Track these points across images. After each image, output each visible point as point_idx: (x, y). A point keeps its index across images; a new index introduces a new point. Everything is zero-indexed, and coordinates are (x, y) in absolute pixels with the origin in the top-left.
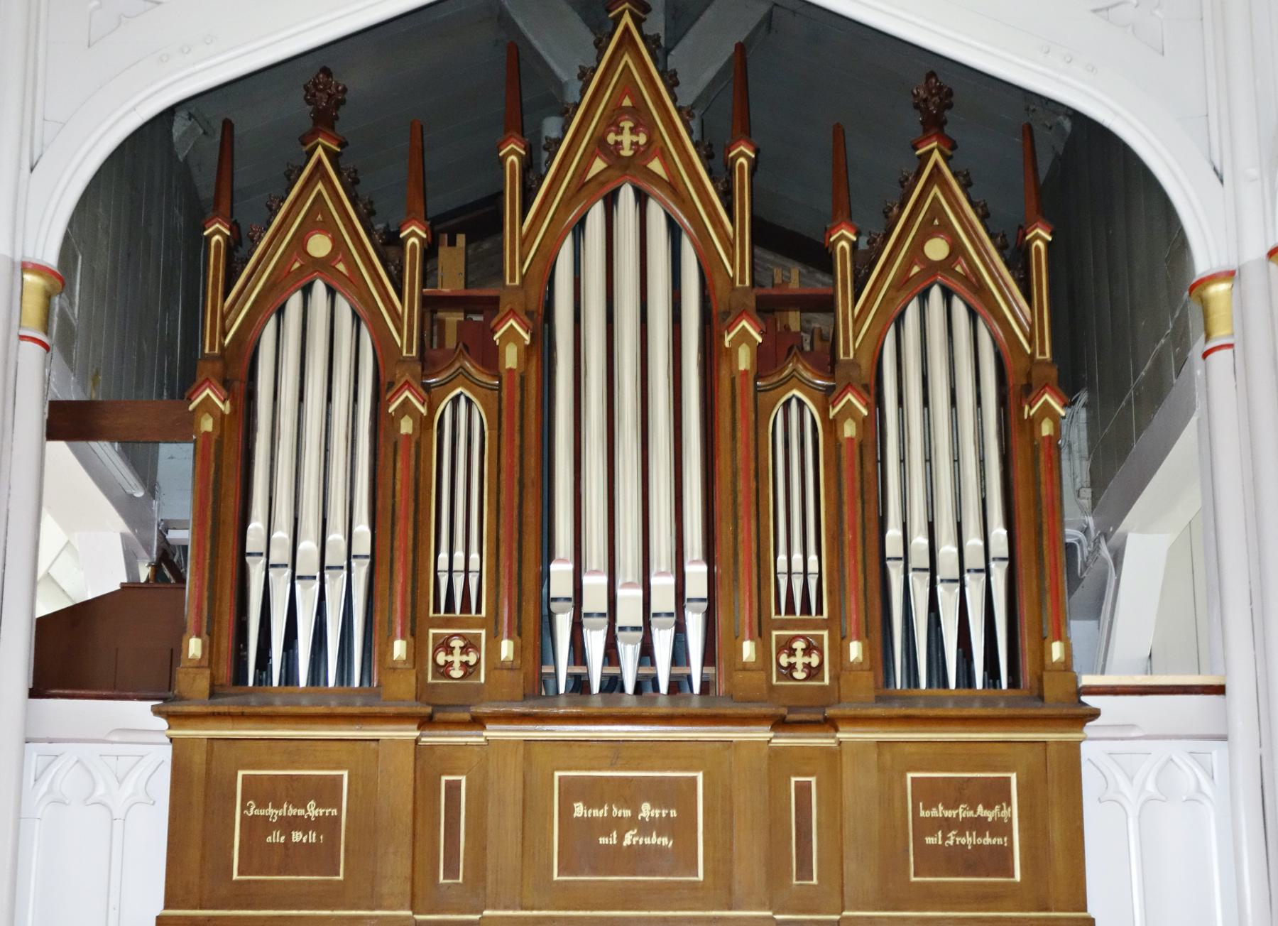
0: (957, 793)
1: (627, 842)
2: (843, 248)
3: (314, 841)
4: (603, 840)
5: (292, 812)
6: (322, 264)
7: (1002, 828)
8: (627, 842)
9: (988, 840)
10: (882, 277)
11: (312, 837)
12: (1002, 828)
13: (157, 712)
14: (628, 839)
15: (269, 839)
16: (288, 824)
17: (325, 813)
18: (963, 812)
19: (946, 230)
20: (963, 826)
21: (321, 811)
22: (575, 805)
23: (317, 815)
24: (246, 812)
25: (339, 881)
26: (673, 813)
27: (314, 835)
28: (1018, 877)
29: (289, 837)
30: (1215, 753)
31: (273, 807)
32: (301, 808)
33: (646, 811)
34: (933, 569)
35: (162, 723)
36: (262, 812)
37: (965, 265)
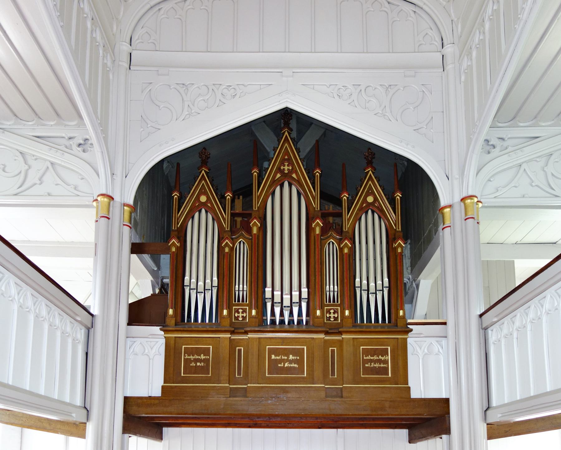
0: (374, 352)
1: (286, 366)
2: (398, 198)
4: (279, 365)
5: (197, 357)
6: (204, 205)
7: (386, 362)
8: (286, 366)
9: (382, 365)
10: (356, 207)
11: (202, 364)
12: (386, 362)
13: (161, 329)
15: (191, 365)
16: (196, 361)
18: (375, 358)
19: (373, 194)
20: (375, 361)
21: (205, 357)
24: (185, 357)
29: (196, 364)
33: (291, 357)
34: (368, 290)
35: (162, 333)
36: (189, 357)
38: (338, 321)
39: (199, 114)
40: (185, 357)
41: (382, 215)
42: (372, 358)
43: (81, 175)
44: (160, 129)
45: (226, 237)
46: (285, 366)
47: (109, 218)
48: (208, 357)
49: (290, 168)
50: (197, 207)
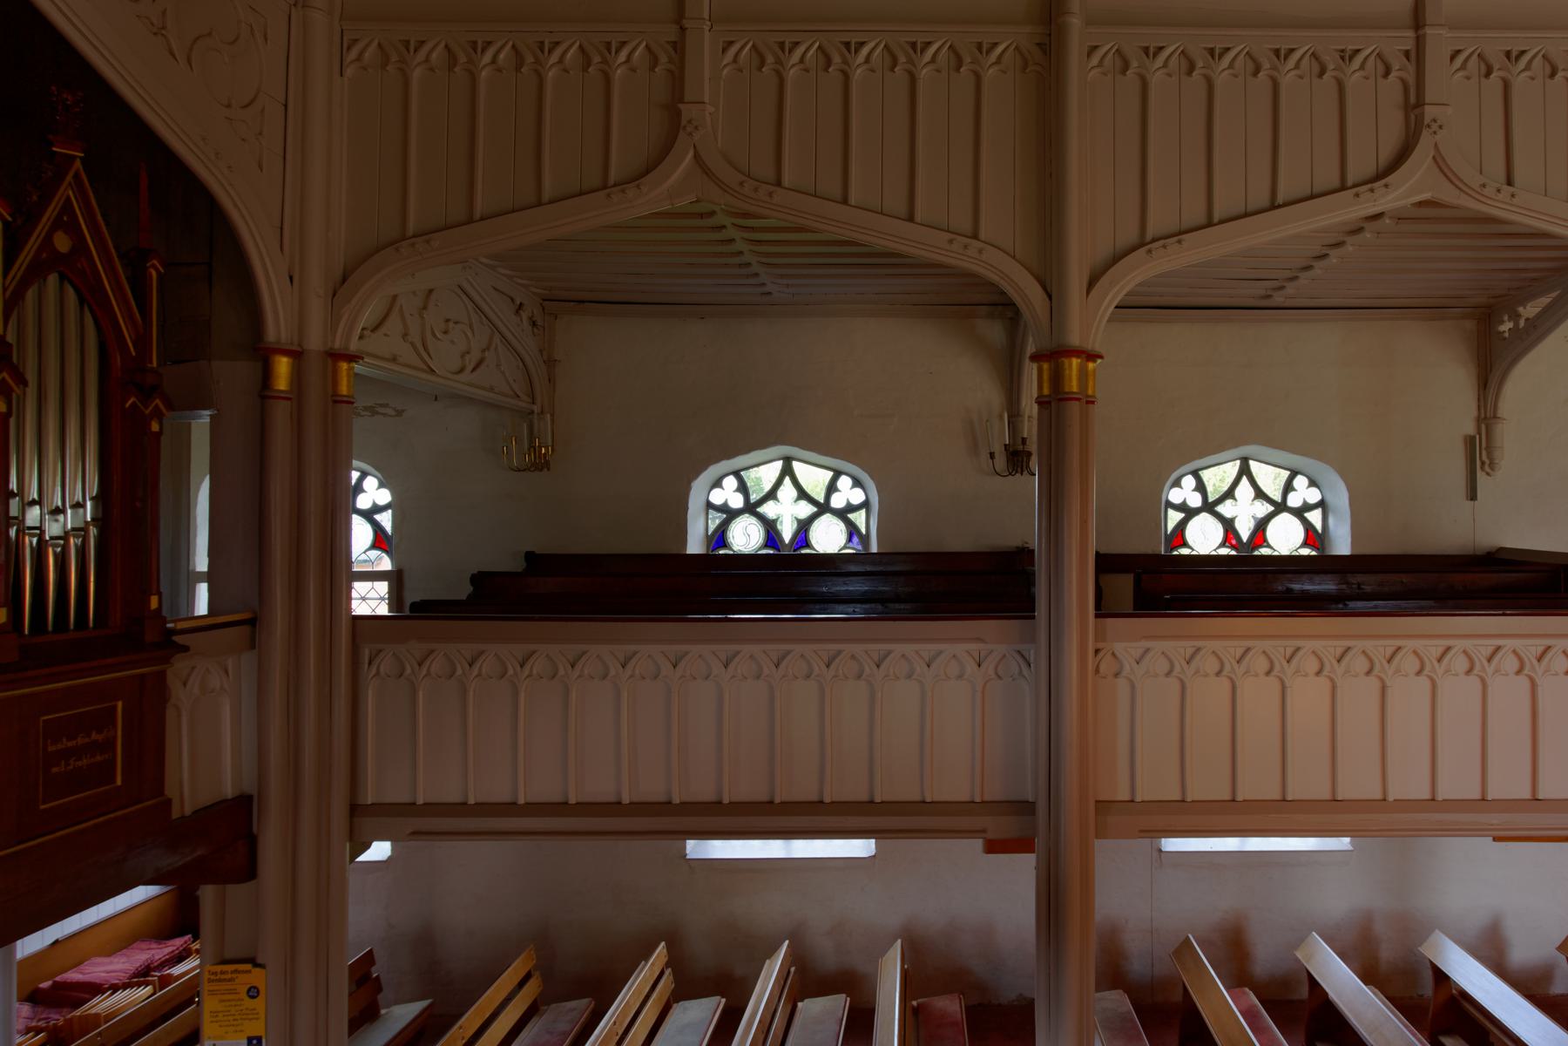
9: (99, 758)
18: (80, 741)
28: (119, 782)
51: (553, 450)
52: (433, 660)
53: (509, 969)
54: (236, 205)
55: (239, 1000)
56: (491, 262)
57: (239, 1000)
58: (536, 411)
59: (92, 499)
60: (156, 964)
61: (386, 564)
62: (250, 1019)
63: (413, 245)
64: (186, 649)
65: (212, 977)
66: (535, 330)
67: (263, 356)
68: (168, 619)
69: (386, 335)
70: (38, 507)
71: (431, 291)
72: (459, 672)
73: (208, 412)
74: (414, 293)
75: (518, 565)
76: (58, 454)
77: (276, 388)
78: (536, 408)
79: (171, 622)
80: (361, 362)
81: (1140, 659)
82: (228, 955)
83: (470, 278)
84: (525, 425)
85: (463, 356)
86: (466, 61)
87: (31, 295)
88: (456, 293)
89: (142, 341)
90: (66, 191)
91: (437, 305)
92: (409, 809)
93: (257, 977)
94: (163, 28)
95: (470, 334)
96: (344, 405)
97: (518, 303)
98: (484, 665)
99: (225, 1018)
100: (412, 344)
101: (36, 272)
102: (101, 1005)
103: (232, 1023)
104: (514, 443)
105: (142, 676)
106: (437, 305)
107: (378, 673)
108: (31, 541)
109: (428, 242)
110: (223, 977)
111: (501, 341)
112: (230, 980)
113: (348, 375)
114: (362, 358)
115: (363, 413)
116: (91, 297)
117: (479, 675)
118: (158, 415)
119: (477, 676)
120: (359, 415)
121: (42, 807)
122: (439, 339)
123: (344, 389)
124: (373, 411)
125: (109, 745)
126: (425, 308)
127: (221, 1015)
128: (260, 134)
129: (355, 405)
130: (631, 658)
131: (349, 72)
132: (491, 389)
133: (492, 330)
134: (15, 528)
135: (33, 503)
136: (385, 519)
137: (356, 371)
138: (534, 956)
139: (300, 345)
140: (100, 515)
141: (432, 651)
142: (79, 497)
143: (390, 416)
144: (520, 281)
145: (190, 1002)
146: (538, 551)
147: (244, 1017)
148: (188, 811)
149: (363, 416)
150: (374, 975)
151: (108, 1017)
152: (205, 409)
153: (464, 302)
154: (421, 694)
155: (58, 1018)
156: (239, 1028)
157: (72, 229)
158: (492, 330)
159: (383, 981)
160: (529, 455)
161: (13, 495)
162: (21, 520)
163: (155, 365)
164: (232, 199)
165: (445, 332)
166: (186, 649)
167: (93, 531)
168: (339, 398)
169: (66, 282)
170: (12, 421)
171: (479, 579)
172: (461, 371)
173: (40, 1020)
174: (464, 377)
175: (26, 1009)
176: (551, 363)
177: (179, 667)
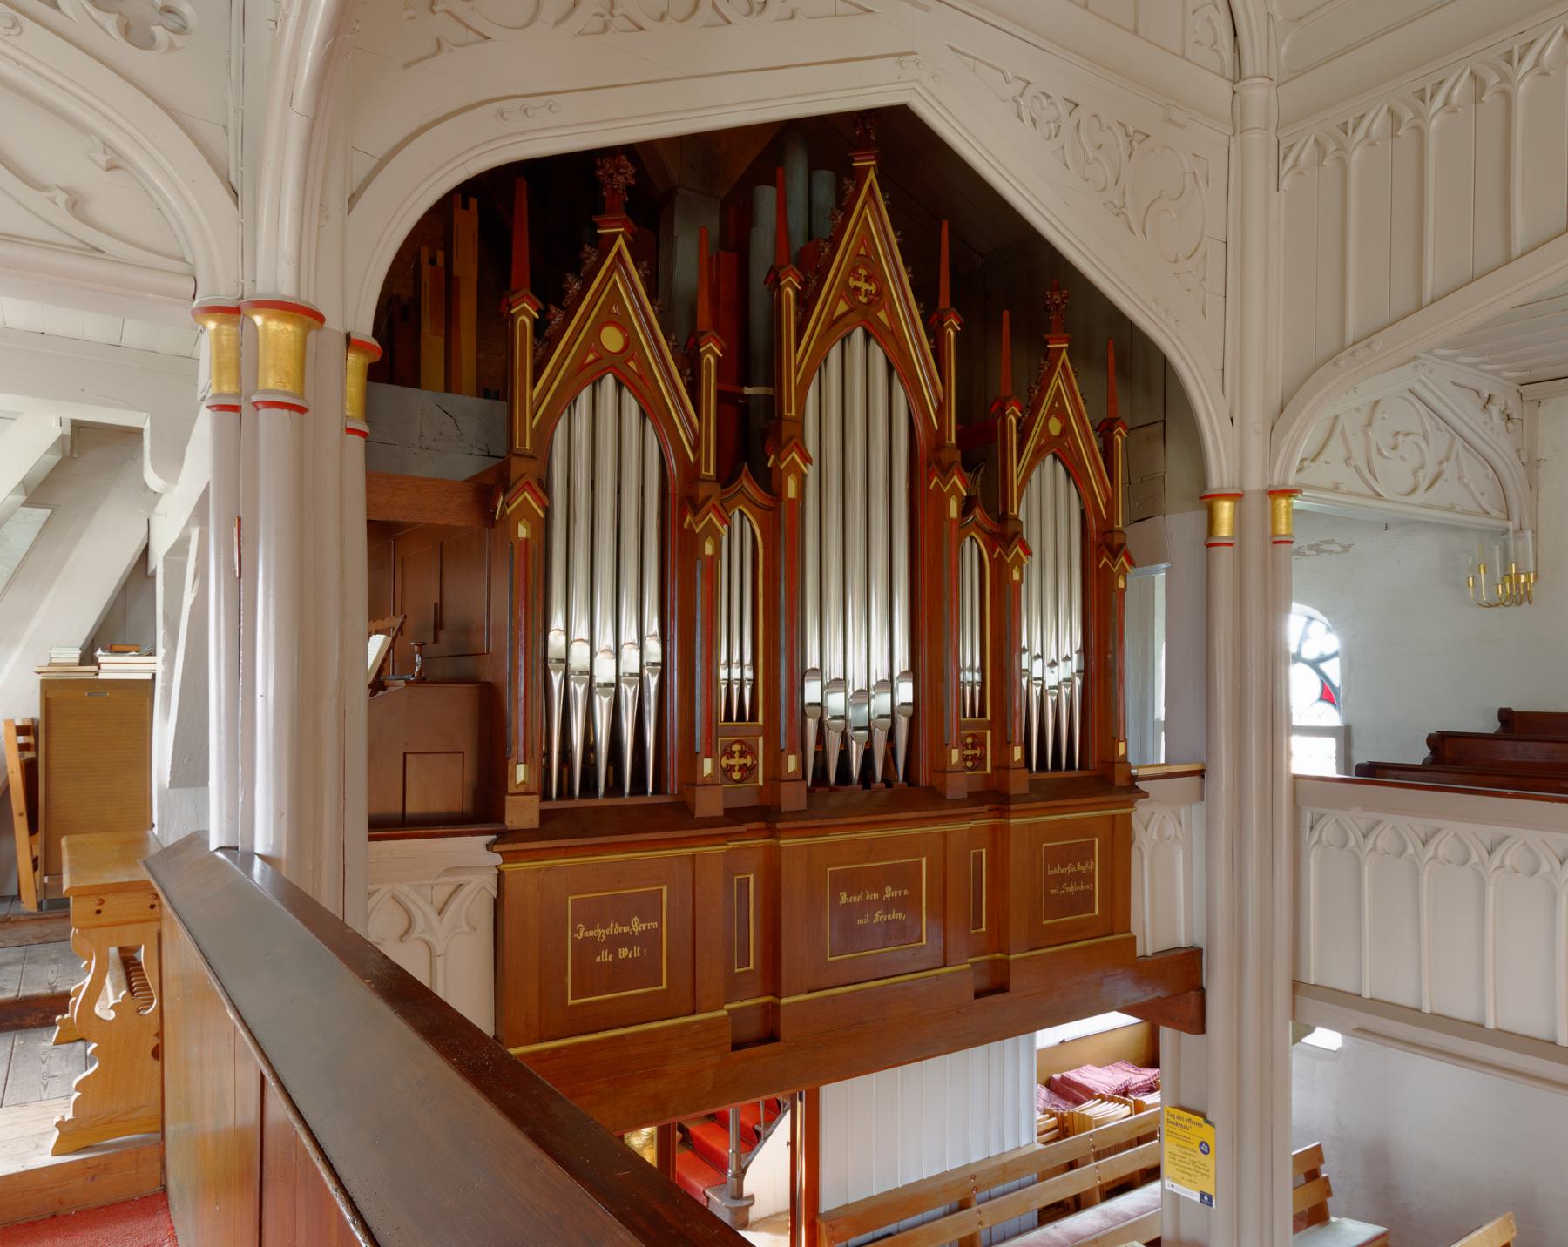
0: (1058, 857)
1: (876, 920)
2: (523, 322)
3: (639, 955)
4: (860, 921)
5: (618, 929)
8: (876, 920)
9: (1082, 887)
11: (637, 951)
13: (489, 847)
14: (878, 918)
15: (598, 959)
16: (615, 942)
17: (647, 927)
18: (1070, 869)
19: (624, 326)
21: (644, 925)
22: (841, 894)
23: (608, 933)
24: (576, 935)
25: (663, 991)
26: (906, 892)
27: (639, 949)
28: (1097, 912)
29: (616, 954)
30: (1183, 810)
31: (601, 928)
32: (627, 925)
33: (889, 893)
36: (591, 934)
37: (1070, 442)
38: (985, 769)
39: (641, 29)
40: (576, 935)
41: (651, 410)
42: (1063, 871)
43: (107, 146)
44: (487, 38)
45: (523, 481)
46: (874, 922)
47: (301, 410)
48: (655, 925)
49: (873, 288)
50: (588, 373)
51: (1536, 577)
52: (1440, 841)
53: (1480, 1231)
54: (1183, 358)
55: (1192, 1150)
56: (1452, 352)
57: (1192, 1150)
58: (1511, 529)
59: (1077, 652)
60: (1133, 1087)
61: (1331, 717)
62: (1203, 1174)
63: (1352, 354)
64: (1145, 795)
65: (1171, 1119)
66: (1510, 425)
67: (1207, 501)
68: (1132, 765)
69: (1327, 463)
70: (1040, 660)
71: (1377, 402)
72: (1410, 850)
73: (1163, 566)
74: (1357, 409)
75: (1491, 726)
76: (1054, 614)
77: (1219, 535)
78: (1510, 525)
79: (1137, 768)
80: (1300, 496)
81: (1368, 834)
82: (1184, 1103)
83: (1422, 378)
84: (517, 446)
85: (1415, 473)
86: (1412, 116)
87: (1034, 476)
88: (1407, 400)
89: (1111, 504)
90: (1057, 381)
91: (1384, 418)
92: (1352, 1000)
93: (1206, 1133)
94: (1124, 207)
95: (1423, 445)
96: (1283, 545)
97: (1486, 396)
98: (1325, 829)
99: (1181, 1164)
100: (1356, 467)
101: (1039, 454)
102: (1092, 1109)
103: (1177, 1162)
104: (1482, 572)
105: (1114, 816)
106: (1384, 418)
107: (1319, 841)
108: (1036, 690)
109: (1368, 346)
110: (1179, 1122)
111: (1464, 447)
112: (1185, 1127)
113: (1287, 513)
114: (1301, 492)
115: (1307, 553)
116: (1075, 472)
117: (1435, 857)
118: (1124, 571)
119: (1431, 859)
120: (1303, 555)
121: (1045, 922)
122: (1385, 457)
123: (1283, 529)
124: (1317, 549)
125: (1089, 878)
126: (1369, 424)
127: (1178, 1158)
128: (1203, 280)
129: (1294, 546)
130: (1499, 844)
131: (1285, 183)
132: (1452, 508)
133: (1452, 435)
134: (1026, 678)
135: (1038, 657)
136: (1333, 670)
137: (1295, 507)
138: (1514, 1227)
139: (1241, 488)
140: (1083, 668)
141: (1379, 823)
142: (1067, 652)
143: (1335, 553)
144: (1488, 367)
145: (1150, 1137)
146: (1516, 708)
147: (1197, 1169)
148: (1149, 953)
149: (1308, 556)
150: (1324, 1175)
151: (1099, 1123)
152: (1161, 563)
153: (1415, 407)
154: (1366, 870)
155: (1065, 1108)
156: (1193, 1179)
157: (1063, 416)
158: (1452, 435)
159: (1332, 1181)
160: (1504, 586)
161: (1025, 650)
162: (1029, 671)
163: (1121, 525)
164: (1180, 352)
165: (1394, 448)
166: (1145, 795)
167: (1078, 682)
168: (1278, 539)
169: (1058, 460)
170: (1023, 587)
171: (1440, 743)
172: (1413, 491)
173: (1053, 1105)
174: (1418, 497)
175: (1044, 1092)
176: (1531, 465)
177: (1140, 813)
